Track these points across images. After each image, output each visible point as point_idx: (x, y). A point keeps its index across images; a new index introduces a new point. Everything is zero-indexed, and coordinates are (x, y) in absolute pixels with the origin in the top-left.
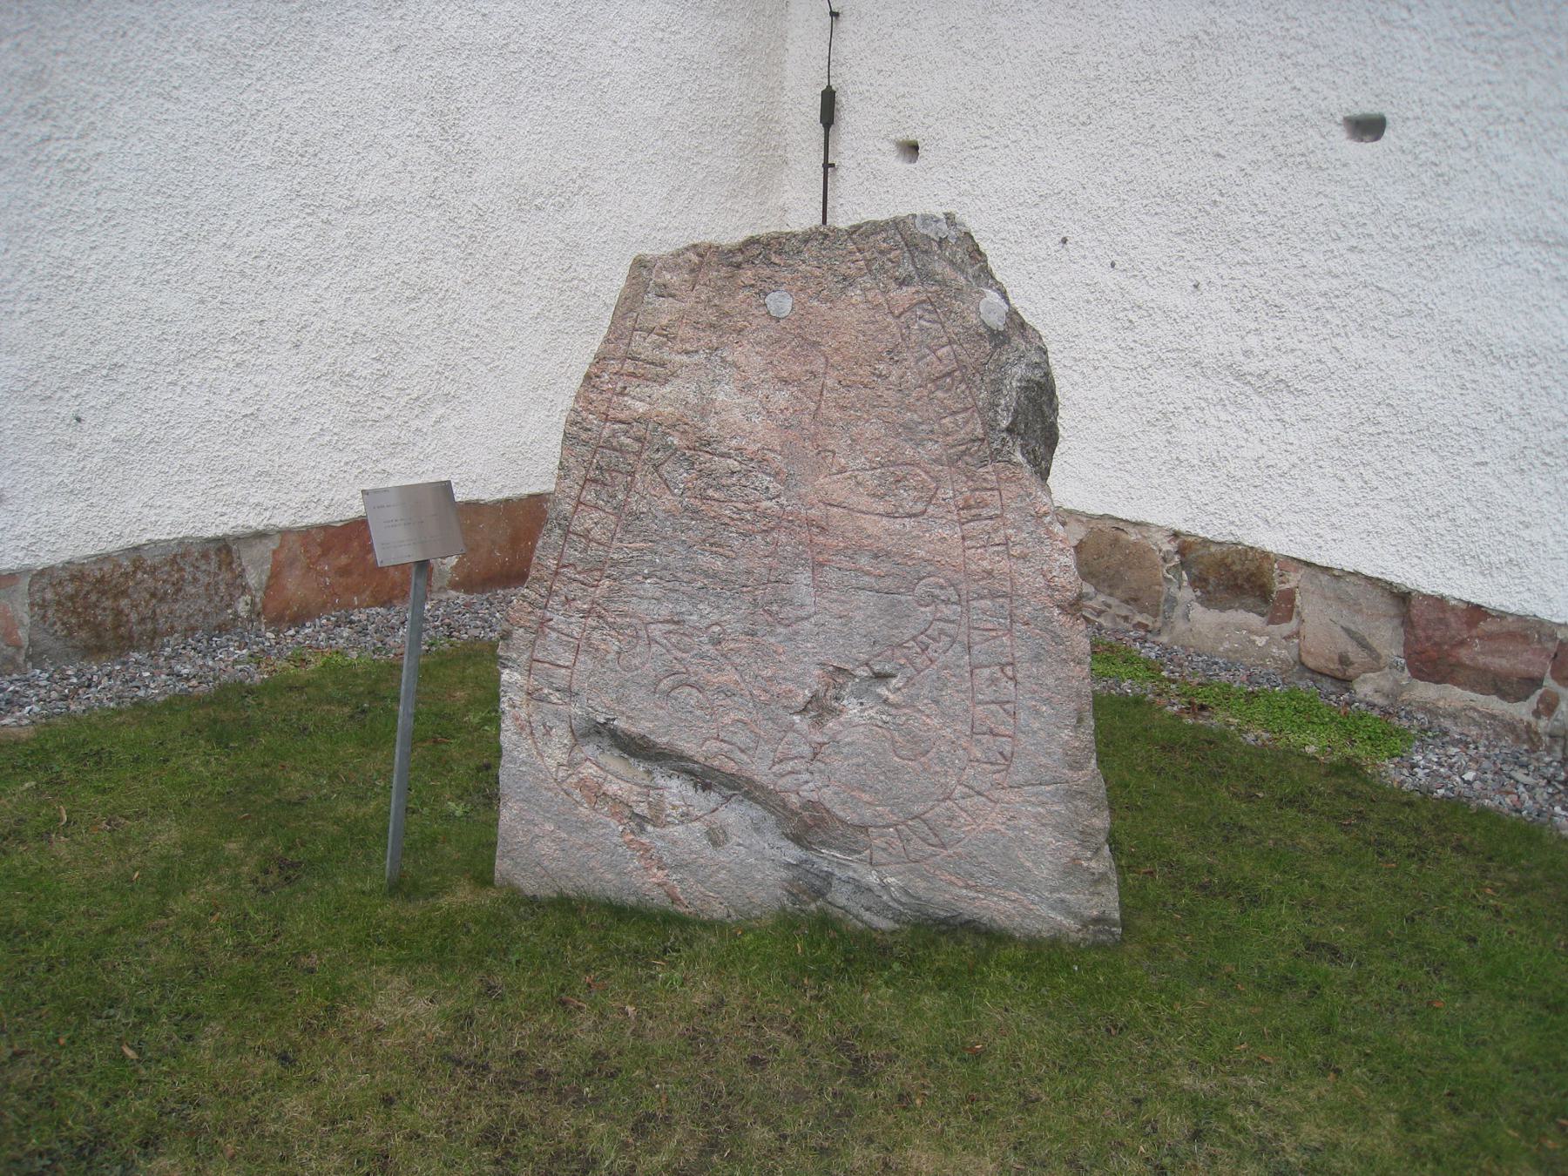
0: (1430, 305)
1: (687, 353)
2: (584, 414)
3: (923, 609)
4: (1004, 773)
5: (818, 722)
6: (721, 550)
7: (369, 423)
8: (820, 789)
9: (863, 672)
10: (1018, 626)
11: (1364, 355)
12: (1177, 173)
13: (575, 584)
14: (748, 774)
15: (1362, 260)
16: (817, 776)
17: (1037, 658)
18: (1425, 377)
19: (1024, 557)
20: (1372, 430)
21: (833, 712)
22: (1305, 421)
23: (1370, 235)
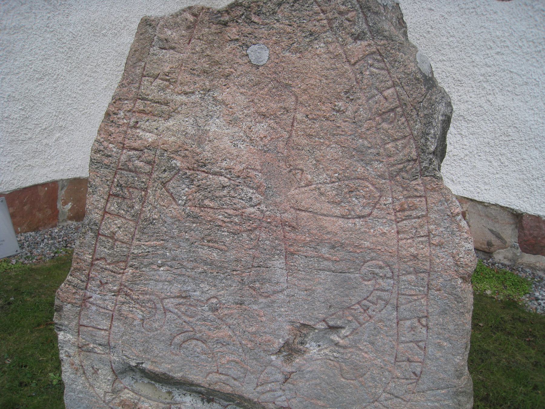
0: (538, 80)
1: (186, 94)
2: (105, 144)
3: (366, 283)
4: (414, 384)
5: (289, 359)
6: (216, 245)
7: (20, 142)
8: (289, 400)
9: (321, 326)
10: (433, 292)
11: (503, 104)
12: (410, 18)
13: (106, 272)
14: (240, 393)
15: (503, 58)
16: (287, 392)
17: (443, 312)
18: (534, 114)
19: (440, 245)
20: (506, 139)
21: (299, 352)
22: (472, 134)
23: (507, 47)
